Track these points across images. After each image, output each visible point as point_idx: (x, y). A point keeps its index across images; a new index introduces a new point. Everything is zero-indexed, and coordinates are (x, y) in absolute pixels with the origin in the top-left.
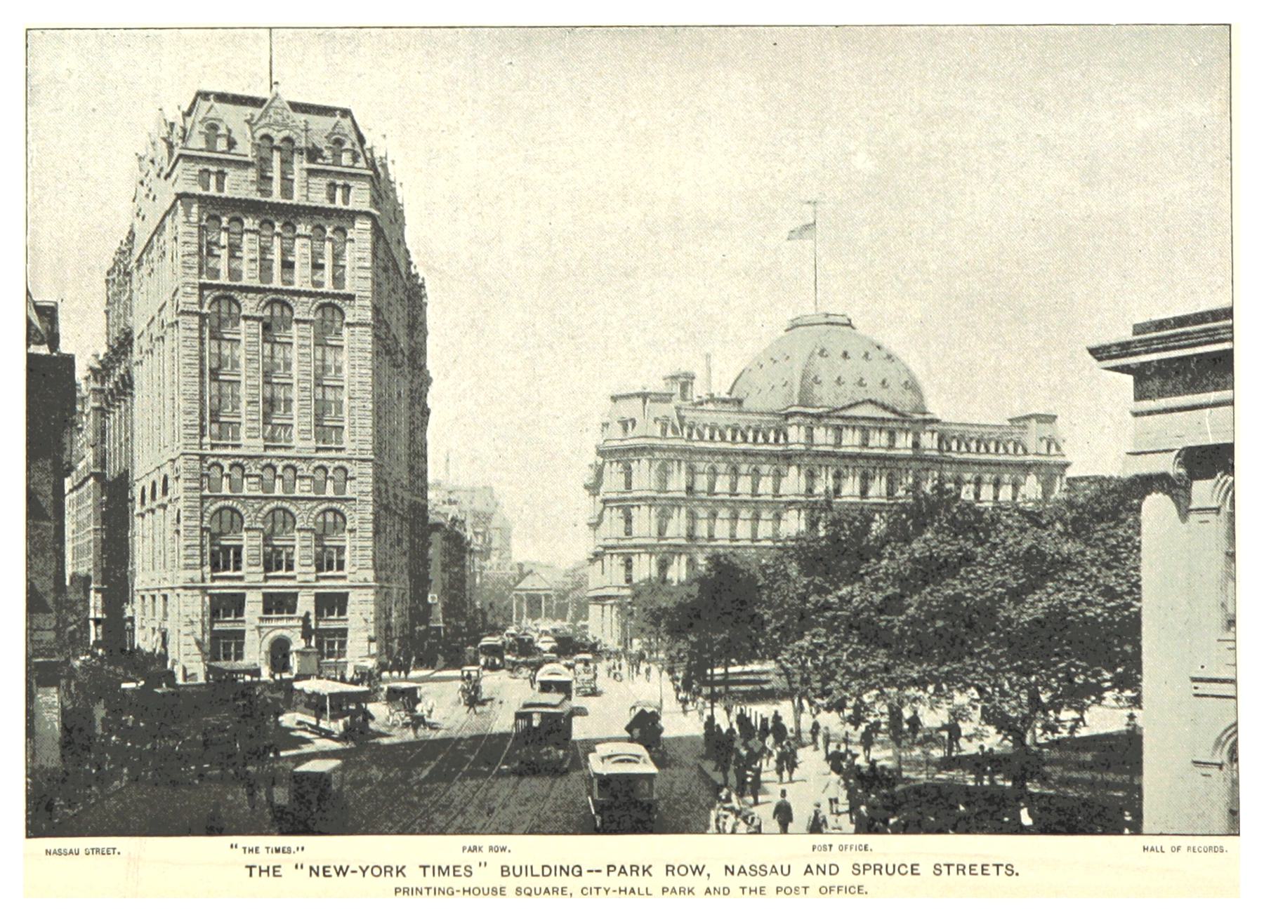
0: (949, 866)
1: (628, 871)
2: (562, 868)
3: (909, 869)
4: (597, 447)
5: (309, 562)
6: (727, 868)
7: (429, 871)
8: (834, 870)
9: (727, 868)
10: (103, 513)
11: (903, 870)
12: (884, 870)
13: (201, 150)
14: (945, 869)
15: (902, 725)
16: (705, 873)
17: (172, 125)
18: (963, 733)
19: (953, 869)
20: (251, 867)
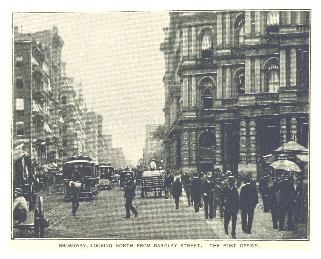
0: (185, 244)
3: (254, 246)
6: (116, 245)
9: (116, 245)
11: (253, 246)
19: (187, 246)
20: (211, 244)
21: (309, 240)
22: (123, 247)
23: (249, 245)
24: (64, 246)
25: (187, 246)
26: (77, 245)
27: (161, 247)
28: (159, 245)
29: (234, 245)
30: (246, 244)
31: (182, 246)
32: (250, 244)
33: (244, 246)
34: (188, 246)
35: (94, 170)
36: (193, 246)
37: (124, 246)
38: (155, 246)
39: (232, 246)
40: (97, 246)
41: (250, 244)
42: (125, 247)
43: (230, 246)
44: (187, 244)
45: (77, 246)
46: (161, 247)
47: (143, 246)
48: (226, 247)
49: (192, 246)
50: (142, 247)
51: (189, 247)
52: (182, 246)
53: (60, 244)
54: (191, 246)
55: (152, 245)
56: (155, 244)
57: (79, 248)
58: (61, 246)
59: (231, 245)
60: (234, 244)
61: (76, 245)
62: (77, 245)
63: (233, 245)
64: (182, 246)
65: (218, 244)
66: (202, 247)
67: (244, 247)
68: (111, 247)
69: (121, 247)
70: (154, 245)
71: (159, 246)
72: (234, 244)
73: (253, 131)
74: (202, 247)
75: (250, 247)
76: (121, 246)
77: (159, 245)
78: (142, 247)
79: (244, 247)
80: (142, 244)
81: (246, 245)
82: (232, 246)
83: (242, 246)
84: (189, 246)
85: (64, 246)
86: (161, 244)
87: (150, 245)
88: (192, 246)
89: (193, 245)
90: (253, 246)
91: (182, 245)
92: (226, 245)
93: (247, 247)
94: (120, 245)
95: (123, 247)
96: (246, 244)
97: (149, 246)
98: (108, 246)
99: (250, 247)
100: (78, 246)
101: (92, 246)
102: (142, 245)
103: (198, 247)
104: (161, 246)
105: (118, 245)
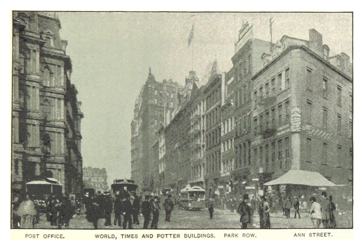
0: (314, 233)
1: (231, 235)
2: (204, 235)
3: (60, 236)
4: (164, 80)
5: (299, 121)
6: (304, 236)
7: (124, 236)
8: (151, 236)
9: (304, 236)
10: (18, 208)
11: (58, 236)
12: (108, 237)
13: (18, 109)
14: (313, 235)
15: (97, 206)
16: (255, 236)
17: (32, 73)
18: (133, 200)
19: (316, 235)
20: (123, 235)
21: (352, 228)
22: (105, 238)
23: (54, 236)
24: (319, 235)
25: (316, 235)
26: (252, 234)
27: (232, 237)
28: (229, 235)
29: (37, 235)
30: (175, 234)
31: (311, 235)
32: (55, 235)
33: (48, 236)
34: (317, 235)
35: (220, 170)
36: (323, 235)
37: (105, 236)
38: (186, 236)
39: (34, 237)
40: (32, 237)
41: (55, 235)
42: (179, 237)
43: (33, 236)
44: (316, 234)
45: (251, 236)
46: (232, 237)
47: (246, 236)
48: (160, 237)
49: (322, 235)
50: (245, 237)
51: (319, 236)
52: (311, 235)
53: (185, 234)
54: (321, 235)
55: (307, 235)
56: (243, 234)
57: (130, 239)
58: (186, 237)
59: (34, 235)
60: (328, 233)
61: (251, 234)
62: (252, 234)
63: (36, 236)
64: (311, 236)
65: (132, 235)
66: (332, 236)
67: (48, 238)
68: (209, 237)
69: (45, 238)
70: (25, 235)
71: (296, 235)
72: (328, 233)
73: (288, 131)
74: (332, 236)
75: (55, 238)
76: (102, 236)
77: (229, 234)
78: (245, 237)
79: (48, 238)
80: (319, 233)
81: (51, 236)
82: (34, 237)
83: (45, 236)
84: (318, 236)
85: (233, 236)
86: (232, 234)
87: (95, 237)
88: (322, 235)
89: (323, 234)
90: (58, 236)
91: (311, 234)
92: (161, 235)
93: (52, 238)
94: (32, 237)
95: (105, 238)
96: (175, 234)
97: (178, 236)
98: (205, 237)
99: (55, 238)
100: (253, 236)
101: (195, 236)
102: (107, 235)
103: (329, 236)
104: (232, 236)
105: (148, 235)
